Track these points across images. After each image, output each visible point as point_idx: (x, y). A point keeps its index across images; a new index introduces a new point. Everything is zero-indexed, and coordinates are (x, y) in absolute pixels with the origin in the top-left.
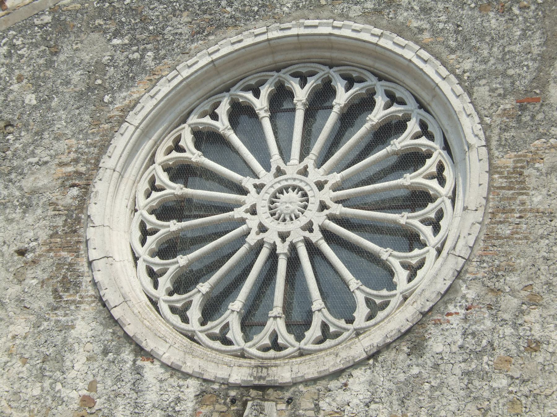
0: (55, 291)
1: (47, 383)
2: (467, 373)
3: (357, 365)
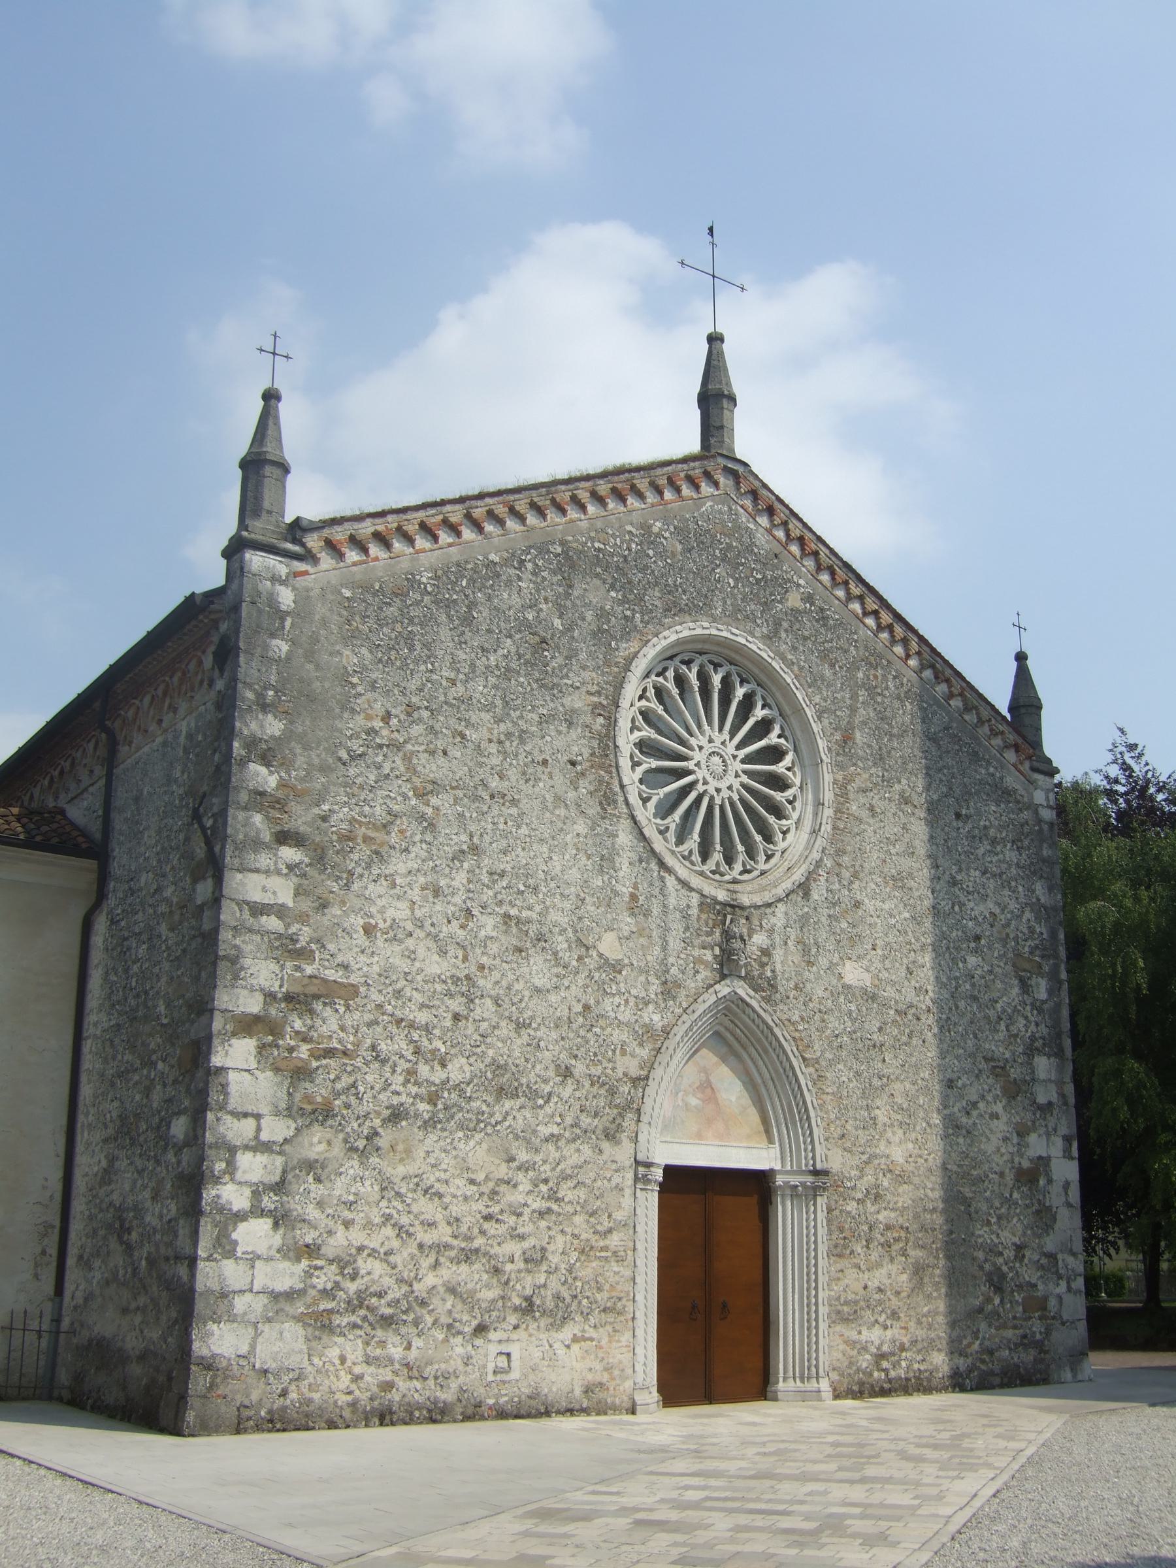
0: (601, 803)
1: (606, 878)
2: (829, 916)
3: (780, 900)
